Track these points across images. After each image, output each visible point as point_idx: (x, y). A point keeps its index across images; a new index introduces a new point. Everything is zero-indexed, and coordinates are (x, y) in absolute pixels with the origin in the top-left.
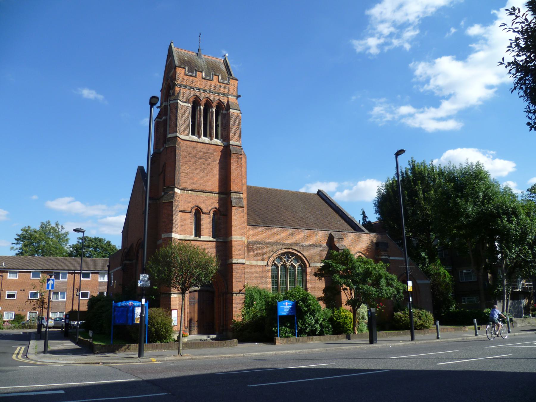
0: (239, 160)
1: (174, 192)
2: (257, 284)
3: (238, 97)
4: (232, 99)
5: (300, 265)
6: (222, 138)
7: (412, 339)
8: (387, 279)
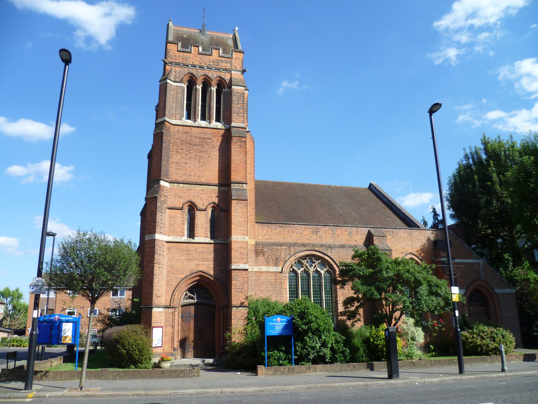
0: (243, 144)
1: (160, 185)
2: (268, 295)
3: (244, 71)
4: (236, 75)
5: (328, 271)
6: (224, 121)
7: (461, 371)
8: (430, 286)
